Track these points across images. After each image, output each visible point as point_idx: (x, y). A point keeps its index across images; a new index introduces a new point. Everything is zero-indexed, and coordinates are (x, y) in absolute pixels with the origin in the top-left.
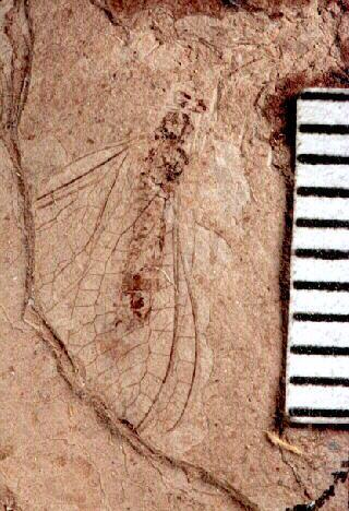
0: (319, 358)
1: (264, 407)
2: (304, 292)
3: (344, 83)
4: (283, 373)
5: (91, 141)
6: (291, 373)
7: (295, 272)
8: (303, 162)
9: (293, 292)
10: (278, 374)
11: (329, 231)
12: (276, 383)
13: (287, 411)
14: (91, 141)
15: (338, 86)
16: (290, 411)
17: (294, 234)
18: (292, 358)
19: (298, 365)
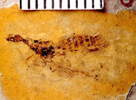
2: (70, 6)
8: (37, 8)
13: (101, 9)
16: (101, 8)
18: (87, 8)
19: (57, 7)
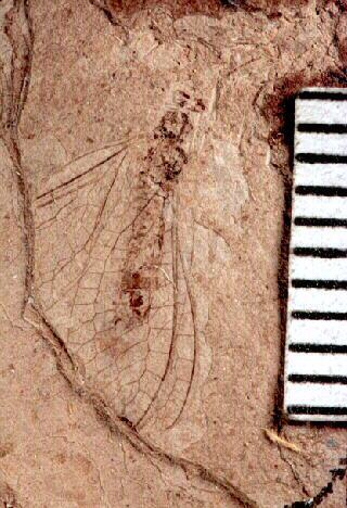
0: (317, 356)
1: (262, 405)
2: (302, 290)
3: (342, 82)
4: (282, 371)
5: (90, 141)
6: (289, 370)
7: (293, 271)
8: (301, 161)
9: (292, 290)
10: (276, 372)
11: (327, 230)
12: (274, 381)
13: (285, 408)
14: (90, 141)
15: (336, 86)
16: (288, 409)
17: (293, 233)
18: (290, 356)
19: (297, 363)
